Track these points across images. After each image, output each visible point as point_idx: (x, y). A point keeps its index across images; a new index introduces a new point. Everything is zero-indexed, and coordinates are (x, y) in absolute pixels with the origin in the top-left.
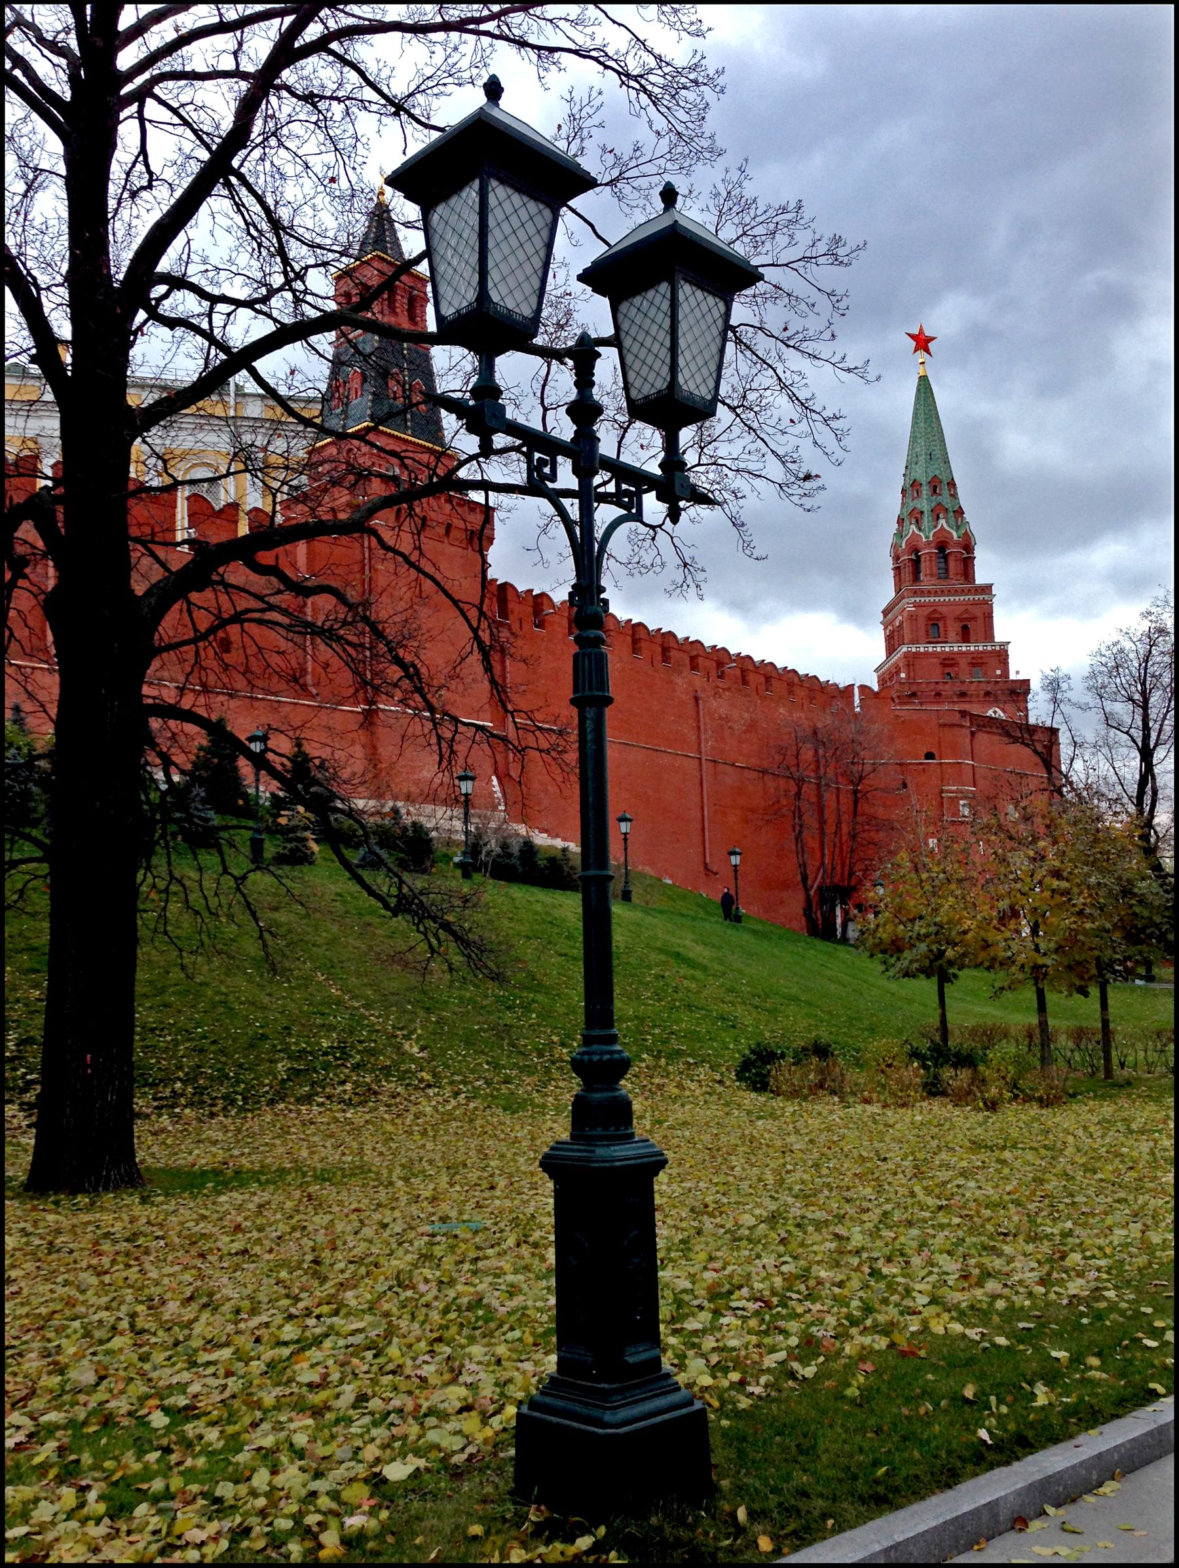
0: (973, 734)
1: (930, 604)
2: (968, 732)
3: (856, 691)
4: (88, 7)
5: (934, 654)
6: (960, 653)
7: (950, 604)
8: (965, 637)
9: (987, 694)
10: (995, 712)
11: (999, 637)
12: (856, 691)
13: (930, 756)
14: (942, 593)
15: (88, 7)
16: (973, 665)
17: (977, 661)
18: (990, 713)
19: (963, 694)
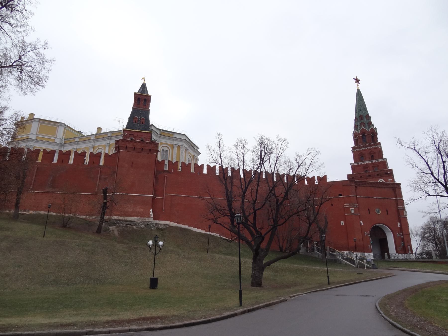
0: (356, 187)
1: (359, 151)
2: (354, 187)
3: (41, 155)
4: (306, 184)
5: (361, 165)
6: (369, 164)
7: (366, 150)
8: (372, 158)
9: (378, 175)
10: (381, 180)
11: (384, 157)
12: (41, 155)
13: (340, 195)
14: (364, 147)
15: (306, 184)
16: (374, 167)
17: (375, 166)
18: (379, 181)
19: (370, 176)
